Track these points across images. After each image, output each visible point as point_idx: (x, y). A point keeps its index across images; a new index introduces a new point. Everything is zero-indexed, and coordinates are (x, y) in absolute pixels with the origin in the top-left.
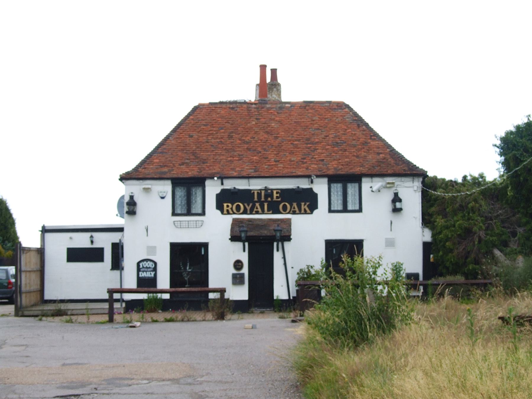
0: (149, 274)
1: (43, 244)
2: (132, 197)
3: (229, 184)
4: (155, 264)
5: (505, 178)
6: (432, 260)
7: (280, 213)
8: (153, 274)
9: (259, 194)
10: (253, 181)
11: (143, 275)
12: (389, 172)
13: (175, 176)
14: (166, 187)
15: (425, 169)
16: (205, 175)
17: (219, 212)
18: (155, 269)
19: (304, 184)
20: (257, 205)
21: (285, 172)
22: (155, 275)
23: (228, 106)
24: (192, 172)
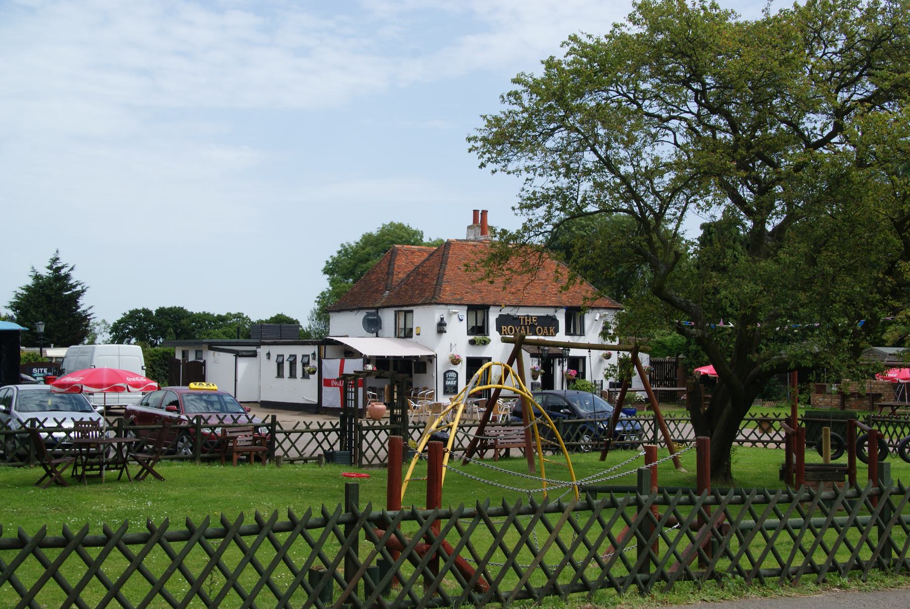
0: (453, 383)
1: (293, 368)
2: (442, 319)
3: (507, 311)
4: (457, 374)
5: (845, 580)
6: (760, 161)
7: (536, 335)
8: (455, 382)
9: (524, 319)
10: (521, 309)
11: (448, 383)
12: (603, 306)
13: (469, 303)
14: (462, 312)
15: (178, 305)
16: (490, 303)
17: (498, 333)
18: (457, 379)
19: (550, 312)
20: (523, 327)
21: (538, 303)
22: (457, 383)
23: (464, 242)
24: (478, 301)
